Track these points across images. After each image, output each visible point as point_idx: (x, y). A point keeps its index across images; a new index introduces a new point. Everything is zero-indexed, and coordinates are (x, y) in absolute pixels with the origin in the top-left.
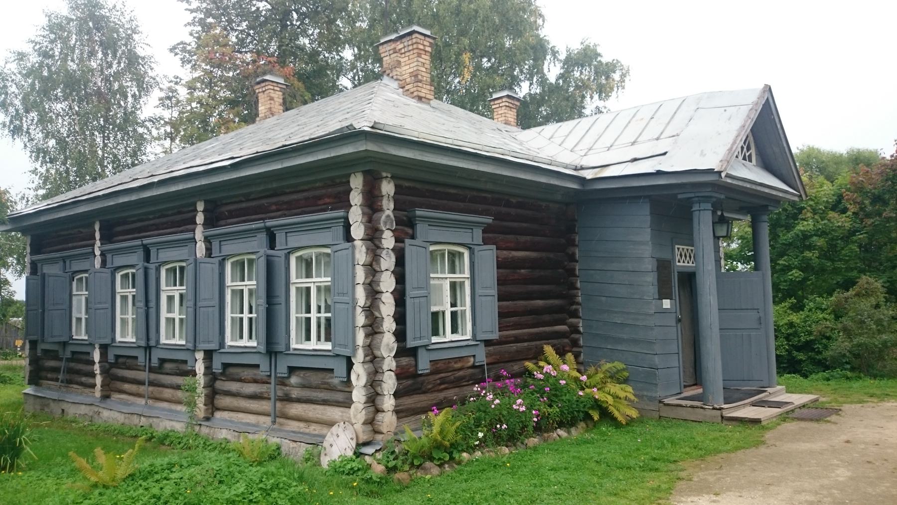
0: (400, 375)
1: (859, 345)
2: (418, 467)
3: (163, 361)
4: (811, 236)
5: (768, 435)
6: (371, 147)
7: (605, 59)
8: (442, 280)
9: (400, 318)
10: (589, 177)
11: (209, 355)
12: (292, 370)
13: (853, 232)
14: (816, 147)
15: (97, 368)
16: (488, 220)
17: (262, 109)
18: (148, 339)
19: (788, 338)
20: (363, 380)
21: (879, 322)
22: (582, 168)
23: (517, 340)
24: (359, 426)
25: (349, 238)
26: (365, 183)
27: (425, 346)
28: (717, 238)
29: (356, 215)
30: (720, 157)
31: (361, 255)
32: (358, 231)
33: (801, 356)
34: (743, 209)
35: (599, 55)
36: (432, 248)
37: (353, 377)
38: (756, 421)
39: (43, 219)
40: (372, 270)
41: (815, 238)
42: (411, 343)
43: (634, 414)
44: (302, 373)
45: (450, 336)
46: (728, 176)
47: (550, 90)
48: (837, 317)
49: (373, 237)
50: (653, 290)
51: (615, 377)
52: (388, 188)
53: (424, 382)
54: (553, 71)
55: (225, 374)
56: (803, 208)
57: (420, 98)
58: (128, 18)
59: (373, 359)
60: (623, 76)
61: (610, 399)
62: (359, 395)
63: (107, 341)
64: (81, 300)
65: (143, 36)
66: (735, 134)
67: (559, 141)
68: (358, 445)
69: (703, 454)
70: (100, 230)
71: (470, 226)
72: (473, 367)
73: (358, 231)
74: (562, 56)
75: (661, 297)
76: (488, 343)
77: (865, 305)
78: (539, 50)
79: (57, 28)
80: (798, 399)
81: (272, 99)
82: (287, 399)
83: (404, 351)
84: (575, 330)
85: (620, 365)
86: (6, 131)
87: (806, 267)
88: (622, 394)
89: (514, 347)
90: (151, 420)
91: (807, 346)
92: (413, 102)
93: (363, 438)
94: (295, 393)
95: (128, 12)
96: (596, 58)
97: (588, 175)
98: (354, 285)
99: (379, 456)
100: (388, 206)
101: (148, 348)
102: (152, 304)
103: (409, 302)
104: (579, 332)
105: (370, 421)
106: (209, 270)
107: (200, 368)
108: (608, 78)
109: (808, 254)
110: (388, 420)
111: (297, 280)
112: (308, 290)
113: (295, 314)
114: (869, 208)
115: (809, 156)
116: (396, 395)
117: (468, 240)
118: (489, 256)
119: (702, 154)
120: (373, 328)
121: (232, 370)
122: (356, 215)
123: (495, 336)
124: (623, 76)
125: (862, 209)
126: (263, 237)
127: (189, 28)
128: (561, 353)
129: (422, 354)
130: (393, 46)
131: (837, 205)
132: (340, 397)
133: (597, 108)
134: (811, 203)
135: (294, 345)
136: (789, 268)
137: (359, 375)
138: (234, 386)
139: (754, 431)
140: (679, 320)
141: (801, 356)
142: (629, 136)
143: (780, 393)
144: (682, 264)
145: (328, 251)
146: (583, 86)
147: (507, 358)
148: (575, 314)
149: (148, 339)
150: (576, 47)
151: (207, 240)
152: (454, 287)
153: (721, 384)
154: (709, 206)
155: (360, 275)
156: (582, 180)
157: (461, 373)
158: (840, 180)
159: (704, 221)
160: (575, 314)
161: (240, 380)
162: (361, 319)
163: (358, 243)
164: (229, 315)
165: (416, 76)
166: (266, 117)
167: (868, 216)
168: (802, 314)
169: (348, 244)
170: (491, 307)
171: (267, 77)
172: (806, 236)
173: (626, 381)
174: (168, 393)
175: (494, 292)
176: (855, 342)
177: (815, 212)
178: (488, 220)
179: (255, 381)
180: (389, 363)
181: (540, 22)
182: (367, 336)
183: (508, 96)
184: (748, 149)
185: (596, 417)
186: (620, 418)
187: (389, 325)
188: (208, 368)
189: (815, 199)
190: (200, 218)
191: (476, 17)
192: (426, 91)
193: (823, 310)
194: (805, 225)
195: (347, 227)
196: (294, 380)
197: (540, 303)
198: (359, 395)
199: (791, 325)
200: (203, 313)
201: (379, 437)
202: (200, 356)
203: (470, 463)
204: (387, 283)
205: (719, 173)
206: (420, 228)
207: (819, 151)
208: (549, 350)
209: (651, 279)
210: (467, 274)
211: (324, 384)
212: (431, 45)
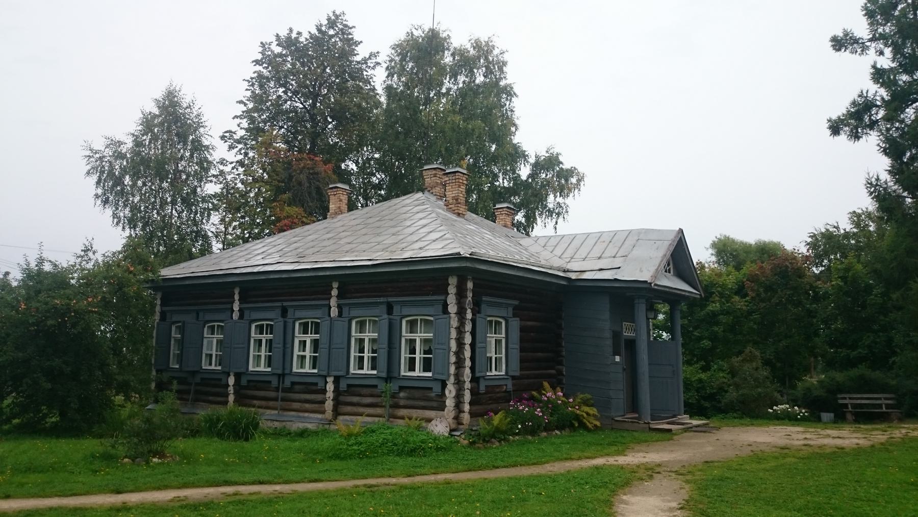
0: (472, 391)
1: (743, 395)
2: (488, 442)
3: (293, 383)
4: (719, 314)
5: (675, 437)
6: (468, 264)
7: (566, 166)
8: (492, 338)
9: (473, 359)
10: (574, 278)
11: (337, 380)
12: (401, 388)
13: (750, 313)
14: (731, 237)
15: (231, 390)
16: (516, 303)
17: (332, 206)
18: (284, 369)
19: (698, 390)
20: (454, 393)
21: (756, 380)
22: (568, 271)
23: (528, 377)
24: (450, 420)
25: (445, 311)
26: (458, 281)
27: (483, 377)
28: (648, 319)
29: (452, 300)
30: (651, 274)
31: (454, 323)
32: (453, 308)
33: (707, 404)
34: (665, 301)
35: (561, 163)
36: (489, 319)
37: (447, 392)
38: (670, 431)
39: (187, 282)
40: (460, 331)
41: (721, 317)
42: (478, 375)
43: (598, 423)
44: (408, 391)
45: (494, 373)
46: (656, 285)
47: (519, 186)
48: (733, 377)
49: (461, 313)
50: (610, 350)
51: (586, 403)
52: (470, 285)
53: (486, 398)
54: (524, 172)
55: (351, 394)
56: (714, 293)
57: (459, 214)
58: (195, 113)
59: (459, 383)
60: (579, 181)
61: (585, 415)
62: (450, 402)
63: (243, 370)
64: (212, 342)
65: (207, 129)
66: (660, 259)
67: (551, 249)
68: (451, 430)
69: (640, 442)
70: (239, 293)
71: (508, 305)
72: (506, 391)
73: (453, 308)
74: (532, 160)
75: (615, 354)
76: (513, 378)
77: (747, 367)
78: (517, 155)
79: (148, 123)
80: (695, 422)
81: (341, 200)
82: (397, 406)
83: (475, 380)
84: (560, 373)
85: (589, 396)
86: (99, 202)
87: (714, 338)
88: (591, 412)
89: (526, 381)
90: (284, 423)
91: (711, 397)
92: (454, 217)
93: (453, 426)
94: (402, 403)
95: (196, 108)
96: (558, 165)
97: (573, 276)
98: (450, 339)
99: (463, 436)
100: (470, 295)
101: (281, 376)
102: (289, 345)
103: (477, 350)
104: (563, 375)
105: (456, 418)
106: (340, 325)
107: (330, 387)
108: (567, 180)
109: (716, 329)
110: (466, 417)
111: (406, 334)
112: (305, 342)
113: (404, 355)
114: (763, 295)
115: (724, 245)
116: (471, 404)
117: (505, 315)
118: (515, 323)
119: (641, 271)
120: (459, 364)
121: (353, 389)
122: (452, 300)
123: (517, 374)
124: (579, 181)
125: (758, 295)
126: (384, 308)
127: (238, 121)
128: (554, 388)
129: (482, 381)
130: (434, 172)
131: (740, 290)
132: (435, 404)
133: (559, 203)
134: (719, 289)
135: (403, 373)
136: (700, 339)
137: (451, 391)
138: (355, 399)
139: (668, 435)
140: (624, 370)
141: (707, 404)
142: (596, 252)
143: (685, 419)
144: (627, 334)
145: (432, 319)
146: (547, 184)
147: (524, 386)
148: (560, 363)
149: (284, 369)
150: (543, 154)
151: (340, 307)
152: (498, 342)
153: (649, 412)
154: (644, 301)
155: (454, 334)
156: (569, 279)
157: (498, 395)
158: (745, 270)
159: (641, 309)
160: (560, 363)
161: (360, 395)
162: (453, 359)
163: (453, 316)
164: (353, 354)
165: (457, 200)
166: (336, 214)
167: (762, 301)
168: (709, 373)
169: (445, 316)
170: (516, 354)
171: (339, 185)
172: (714, 315)
173: (592, 405)
174: (296, 405)
175: (518, 347)
176: (740, 392)
177: (721, 295)
178: (516, 303)
179: (372, 396)
180: (468, 385)
181: (513, 129)
182: (456, 368)
183: (508, 207)
184: (669, 265)
185: (577, 425)
186: (590, 426)
187: (468, 363)
188: (336, 390)
189: (723, 286)
190: (335, 292)
191: (472, 134)
192: (462, 209)
193: (723, 371)
194: (714, 307)
195: (445, 306)
196: (402, 394)
197: (540, 354)
198: (450, 402)
199: (700, 381)
200: (330, 352)
201: (461, 427)
202: (330, 380)
203: (513, 441)
204: (468, 339)
205: (651, 283)
206: (483, 306)
207: (733, 241)
208: (546, 384)
209: (609, 342)
210: (503, 335)
211: (427, 397)
212: (467, 180)
